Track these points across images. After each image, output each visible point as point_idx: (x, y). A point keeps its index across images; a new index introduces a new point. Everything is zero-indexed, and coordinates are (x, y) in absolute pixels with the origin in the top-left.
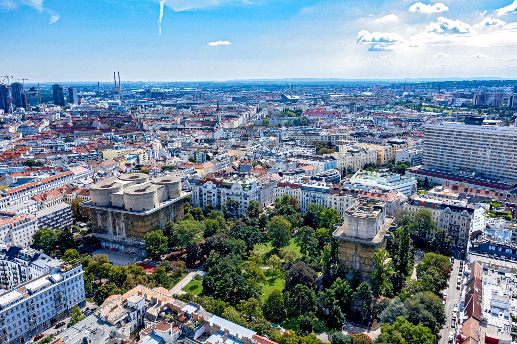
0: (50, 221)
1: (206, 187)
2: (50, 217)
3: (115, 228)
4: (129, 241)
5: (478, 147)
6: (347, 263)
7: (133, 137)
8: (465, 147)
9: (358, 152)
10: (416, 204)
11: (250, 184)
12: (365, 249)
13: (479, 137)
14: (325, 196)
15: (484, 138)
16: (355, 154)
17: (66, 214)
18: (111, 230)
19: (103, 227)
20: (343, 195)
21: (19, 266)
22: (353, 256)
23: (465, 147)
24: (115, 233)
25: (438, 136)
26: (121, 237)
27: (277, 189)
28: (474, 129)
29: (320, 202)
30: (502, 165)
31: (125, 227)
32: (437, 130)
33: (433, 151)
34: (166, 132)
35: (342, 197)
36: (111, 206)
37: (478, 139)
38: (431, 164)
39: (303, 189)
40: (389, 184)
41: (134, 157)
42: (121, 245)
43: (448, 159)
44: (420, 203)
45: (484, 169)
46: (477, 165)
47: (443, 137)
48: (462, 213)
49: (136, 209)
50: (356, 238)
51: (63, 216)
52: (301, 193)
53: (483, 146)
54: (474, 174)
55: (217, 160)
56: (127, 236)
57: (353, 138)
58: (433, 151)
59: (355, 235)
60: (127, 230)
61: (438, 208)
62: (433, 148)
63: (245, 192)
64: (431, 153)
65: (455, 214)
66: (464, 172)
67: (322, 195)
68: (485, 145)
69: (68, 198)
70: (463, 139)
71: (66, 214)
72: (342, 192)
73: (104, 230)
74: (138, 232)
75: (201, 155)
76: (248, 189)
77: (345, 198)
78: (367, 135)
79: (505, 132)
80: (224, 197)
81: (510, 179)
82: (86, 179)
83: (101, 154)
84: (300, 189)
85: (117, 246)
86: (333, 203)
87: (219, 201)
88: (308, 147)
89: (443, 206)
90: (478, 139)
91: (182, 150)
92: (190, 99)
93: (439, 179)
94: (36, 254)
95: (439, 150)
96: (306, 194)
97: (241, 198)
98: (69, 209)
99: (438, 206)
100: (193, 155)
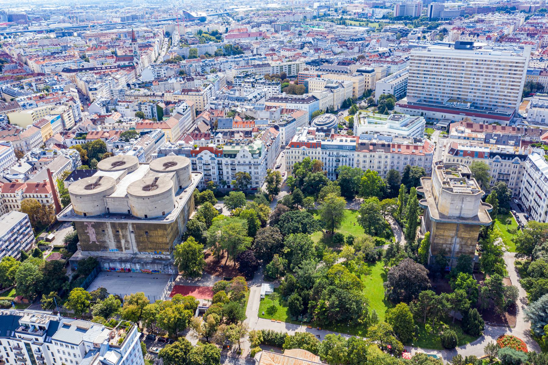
0: (7, 243)
1: (201, 158)
2: (6, 238)
3: (119, 242)
4: (143, 256)
5: (471, 74)
6: (444, 245)
7: (31, 86)
8: (455, 75)
9: (337, 87)
10: (461, 155)
11: (258, 149)
12: (469, 229)
13: (472, 64)
14: (352, 153)
15: (477, 64)
16: (335, 91)
17: (24, 228)
18: (112, 244)
19: (99, 242)
20: (374, 151)
21: (27, 345)
22: (452, 237)
23: (455, 75)
24: (119, 248)
25: (425, 64)
26: (130, 251)
27: (290, 151)
28: (467, 55)
29: (346, 160)
30: (496, 93)
31: (136, 238)
32: (425, 57)
33: (420, 81)
34: (74, 74)
35: (373, 154)
36: (108, 214)
37: (471, 65)
38: (416, 95)
39: (324, 147)
40: (404, 128)
41: (58, 118)
42: (135, 263)
43: (436, 89)
44: (465, 153)
47: (431, 64)
48: (513, 160)
49: (154, 215)
50: (460, 218)
51: (21, 231)
52: (321, 153)
53: (476, 73)
54: (469, 104)
55: (178, 113)
56: (140, 251)
57: (309, 67)
58: (420, 81)
59: (458, 215)
60: (138, 242)
61: (486, 157)
62: (420, 77)
63: (255, 160)
64: (417, 84)
66: (459, 103)
68: (479, 71)
69: (7, 199)
70: (454, 66)
71: (24, 228)
72: (371, 147)
73: (100, 246)
74: (157, 243)
75: (150, 107)
76: (258, 155)
77: (376, 154)
78: (324, 62)
79: (500, 57)
80: (227, 168)
81: (503, 106)
82: (20, 166)
83: (6, 118)
84: (319, 149)
85: (128, 266)
86: (361, 161)
87: (220, 174)
88: (273, 84)
89: (492, 155)
90: (471, 65)
91: (119, 101)
92: (64, 22)
93: (434, 112)
94: (51, 322)
95: (426, 79)
96: (328, 153)
97: (250, 168)
98: (27, 220)
99: (486, 155)
100: (137, 108)
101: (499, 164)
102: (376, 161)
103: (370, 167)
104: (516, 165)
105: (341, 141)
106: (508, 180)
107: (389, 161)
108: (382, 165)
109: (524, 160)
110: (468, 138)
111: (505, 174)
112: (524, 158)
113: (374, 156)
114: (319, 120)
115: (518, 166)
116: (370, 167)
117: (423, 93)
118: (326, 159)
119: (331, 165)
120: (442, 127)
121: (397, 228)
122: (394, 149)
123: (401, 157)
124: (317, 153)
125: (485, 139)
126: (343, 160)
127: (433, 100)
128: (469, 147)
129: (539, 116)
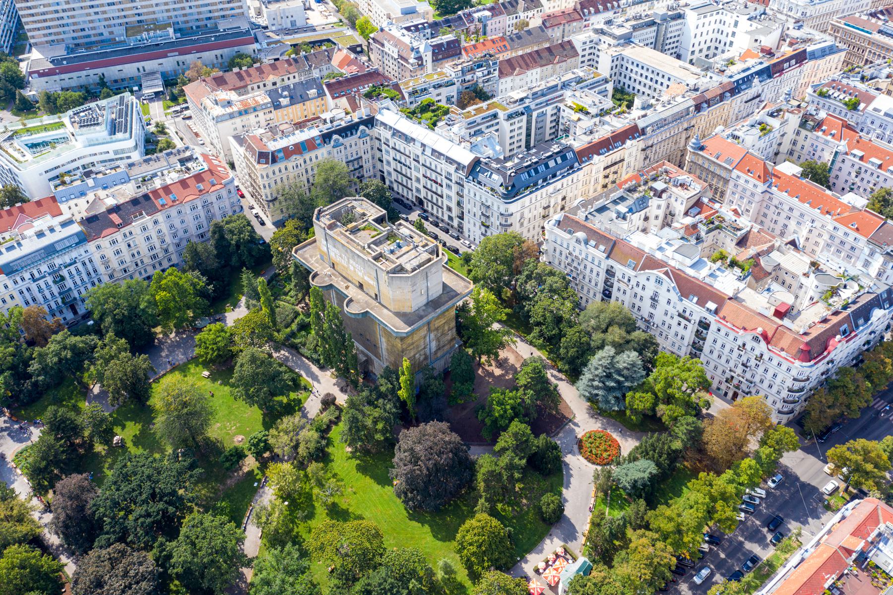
14: (81, 250)
20: (126, 223)
29: (77, 270)
35: (126, 230)
40: (119, 135)
44: (288, 153)
45: (172, 14)
46: (155, 9)
65: (348, 141)
66: (152, 33)
67: (74, 254)
72: (115, 218)
96: (27, 276)
99: (318, 142)
101: (342, 148)
102: (139, 241)
103: (133, 255)
105: (40, 234)
106: (362, 167)
107: (164, 227)
109: (372, 126)
110: (246, 112)
111: (355, 160)
112: (370, 122)
113: (131, 233)
116: (133, 255)
117: (66, 29)
118: (28, 290)
119: (49, 296)
120: (156, 93)
122: (161, 201)
125: (273, 102)
126: (70, 273)
127: (93, 39)
129: (285, 18)
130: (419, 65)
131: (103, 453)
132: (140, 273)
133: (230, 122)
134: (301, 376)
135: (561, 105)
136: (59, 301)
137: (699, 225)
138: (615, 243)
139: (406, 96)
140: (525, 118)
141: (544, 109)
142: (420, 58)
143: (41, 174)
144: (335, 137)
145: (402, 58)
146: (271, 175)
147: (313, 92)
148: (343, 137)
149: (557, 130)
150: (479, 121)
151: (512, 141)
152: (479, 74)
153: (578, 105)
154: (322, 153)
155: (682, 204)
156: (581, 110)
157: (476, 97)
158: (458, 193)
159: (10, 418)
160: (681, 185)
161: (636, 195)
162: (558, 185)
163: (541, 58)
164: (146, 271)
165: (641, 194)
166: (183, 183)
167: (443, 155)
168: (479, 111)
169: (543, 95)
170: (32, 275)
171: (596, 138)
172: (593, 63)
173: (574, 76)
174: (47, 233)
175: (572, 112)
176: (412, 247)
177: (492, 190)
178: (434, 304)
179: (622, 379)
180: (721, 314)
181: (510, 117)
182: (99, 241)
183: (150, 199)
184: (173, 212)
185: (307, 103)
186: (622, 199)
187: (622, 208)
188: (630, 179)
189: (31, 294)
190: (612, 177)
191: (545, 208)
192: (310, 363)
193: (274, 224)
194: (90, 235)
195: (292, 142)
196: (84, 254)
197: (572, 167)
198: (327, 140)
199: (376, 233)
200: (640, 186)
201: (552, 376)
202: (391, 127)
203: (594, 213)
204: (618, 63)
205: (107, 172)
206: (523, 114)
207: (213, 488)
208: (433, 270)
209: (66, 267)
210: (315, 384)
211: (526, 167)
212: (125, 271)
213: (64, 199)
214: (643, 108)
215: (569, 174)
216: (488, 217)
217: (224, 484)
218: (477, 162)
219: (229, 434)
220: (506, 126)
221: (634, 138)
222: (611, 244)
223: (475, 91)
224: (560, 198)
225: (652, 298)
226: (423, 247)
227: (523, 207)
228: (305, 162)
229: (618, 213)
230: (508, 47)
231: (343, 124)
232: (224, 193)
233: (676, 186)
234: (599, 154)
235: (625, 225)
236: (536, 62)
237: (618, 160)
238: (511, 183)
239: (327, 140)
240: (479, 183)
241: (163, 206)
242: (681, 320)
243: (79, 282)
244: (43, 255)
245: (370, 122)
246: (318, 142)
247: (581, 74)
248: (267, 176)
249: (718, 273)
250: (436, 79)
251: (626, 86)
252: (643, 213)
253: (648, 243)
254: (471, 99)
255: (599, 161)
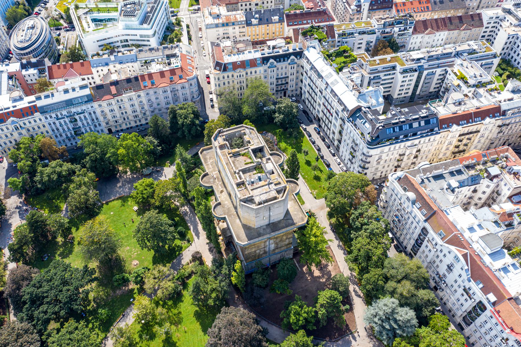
14: (89, 106)
20: (119, 94)
29: (85, 117)
35: (119, 98)
39: (43, 110)
40: (145, 26)
44: (235, 66)
52: (43, 118)
65: (280, 65)
67: (84, 107)
72: (113, 89)
96: (54, 115)
101: (275, 69)
103: (122, 113)
104: (293, 66)
105: (66, 91)
106: (287, 83)
107: (144, 100)
108: (137, 108)
109: (300, 57)
110: (227, 25)
112: (299, 54)
113: (122, 100)
114: (20, 38)
115: (295, 66)
116: (122, 113)
118: (54, 123)
119: (66, 129)
121: (188, 210)
123: (157, 91)
124: (38, 121)
125: (246, 21)
128: (237, 56)
130: (357, 11)
131: (60, 243)
132: (126, 124)
133: (215, 30)
134: (190, 229)
135: (449, 69)
136: (73, 132)
137: (515, 215)
138: (435, 213)
139: (337, 36)
140: (416, 74)
141: (434, 70)
142: (359, 6)
143: (94, 42)
144: (271, 60)
145: (348, 3)
146: (221, 78)
147: (276, 18)
148: (277, 62)
149: (441, 86)
150: (380, 69)
151: (402, 88)
152: (396, 29)
153: (461, 74)
154: (260, 70)
155: (509, 189)
156: (463, 79)
157: (389, 46)
158: (341, 125)
159: (24, 201)
160: (514, 173)
161: (472, 172)
162: (416, 142)
163: (451, 24)
164: (130, 123)
165: (477, 173)
166: (162, 74)
167: (338, 96)
168: (383, 61)
169: (438, 59)
170: (57, 115)
171: (461, 110)
172: (490, 40)
173: (468, 48)
174: (71, 91)
175: (456, 78)
176: (267, 183)
177: (362, 134)
178: (273, 226)
179: (396, 326)
180: (497, 308)
181: (405, 71)
182: (100, 102)
183: (138, 80)
184: (151, 92)
185: (270, 25)
186: (459, 172)
187: (454, 182)
188: (472, 158)
189: (56, 126)
190: (465, 141)
191: (400, 155)
192: (199, 222)
193: (220, 109)
194: (95, 98)
195: (240, 59)
196: (90, 108)
197: (432, 130)
198: (265, 62)
199: (249, 161)
200: (478, 165)
201: (354, 291)
202: (311, 63)
203: (431, 179)
204: (513, 40)
205: (125, 52)
206: (416, 71)
207: (107, 292)
208: (276, 206)
209: (77, 114)
210: (195, 238)
211: (394, 124)
212: (116, 122)
213: (95, 65)
214: (513, 92)
215: (427, 136)
216: (355, 151)
217: (115, 292)
218: (359, 109)
219: (131, 257)
220: (400, 77)
221: (494, 116)
222: (432, 213)
223: (389, 42)
224: (415, 150)
225: (448, 266)
226: (276, 185)
227: (382, 152)
228: (247, 74)
229: (449, 186)
230: (430, 9)
231: (281, 52)
232: (187, 85)
233: (510, 173)
234: (458, 125)
235: (451, 197)
236: (446, 26)
237: (474, 130)
238: (376, 135)
239: (265, 62)
240: (355, 125)
241: (145, 87)
242: (465, 294)
243: (86, 124)
244: (64, 105)
245: (299, 54)
246: (259, 62)
247: (475, 47)
248: (219, 79)
249: (511, 268)
250: (363, 27)
251: (513, 59)
252: (472, 188)
253: (461, 219)
254: (385, 47)
255: (456, 130)
